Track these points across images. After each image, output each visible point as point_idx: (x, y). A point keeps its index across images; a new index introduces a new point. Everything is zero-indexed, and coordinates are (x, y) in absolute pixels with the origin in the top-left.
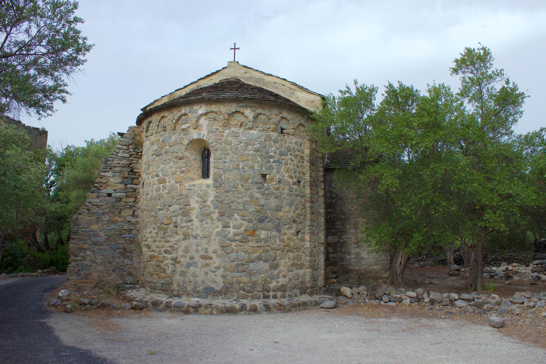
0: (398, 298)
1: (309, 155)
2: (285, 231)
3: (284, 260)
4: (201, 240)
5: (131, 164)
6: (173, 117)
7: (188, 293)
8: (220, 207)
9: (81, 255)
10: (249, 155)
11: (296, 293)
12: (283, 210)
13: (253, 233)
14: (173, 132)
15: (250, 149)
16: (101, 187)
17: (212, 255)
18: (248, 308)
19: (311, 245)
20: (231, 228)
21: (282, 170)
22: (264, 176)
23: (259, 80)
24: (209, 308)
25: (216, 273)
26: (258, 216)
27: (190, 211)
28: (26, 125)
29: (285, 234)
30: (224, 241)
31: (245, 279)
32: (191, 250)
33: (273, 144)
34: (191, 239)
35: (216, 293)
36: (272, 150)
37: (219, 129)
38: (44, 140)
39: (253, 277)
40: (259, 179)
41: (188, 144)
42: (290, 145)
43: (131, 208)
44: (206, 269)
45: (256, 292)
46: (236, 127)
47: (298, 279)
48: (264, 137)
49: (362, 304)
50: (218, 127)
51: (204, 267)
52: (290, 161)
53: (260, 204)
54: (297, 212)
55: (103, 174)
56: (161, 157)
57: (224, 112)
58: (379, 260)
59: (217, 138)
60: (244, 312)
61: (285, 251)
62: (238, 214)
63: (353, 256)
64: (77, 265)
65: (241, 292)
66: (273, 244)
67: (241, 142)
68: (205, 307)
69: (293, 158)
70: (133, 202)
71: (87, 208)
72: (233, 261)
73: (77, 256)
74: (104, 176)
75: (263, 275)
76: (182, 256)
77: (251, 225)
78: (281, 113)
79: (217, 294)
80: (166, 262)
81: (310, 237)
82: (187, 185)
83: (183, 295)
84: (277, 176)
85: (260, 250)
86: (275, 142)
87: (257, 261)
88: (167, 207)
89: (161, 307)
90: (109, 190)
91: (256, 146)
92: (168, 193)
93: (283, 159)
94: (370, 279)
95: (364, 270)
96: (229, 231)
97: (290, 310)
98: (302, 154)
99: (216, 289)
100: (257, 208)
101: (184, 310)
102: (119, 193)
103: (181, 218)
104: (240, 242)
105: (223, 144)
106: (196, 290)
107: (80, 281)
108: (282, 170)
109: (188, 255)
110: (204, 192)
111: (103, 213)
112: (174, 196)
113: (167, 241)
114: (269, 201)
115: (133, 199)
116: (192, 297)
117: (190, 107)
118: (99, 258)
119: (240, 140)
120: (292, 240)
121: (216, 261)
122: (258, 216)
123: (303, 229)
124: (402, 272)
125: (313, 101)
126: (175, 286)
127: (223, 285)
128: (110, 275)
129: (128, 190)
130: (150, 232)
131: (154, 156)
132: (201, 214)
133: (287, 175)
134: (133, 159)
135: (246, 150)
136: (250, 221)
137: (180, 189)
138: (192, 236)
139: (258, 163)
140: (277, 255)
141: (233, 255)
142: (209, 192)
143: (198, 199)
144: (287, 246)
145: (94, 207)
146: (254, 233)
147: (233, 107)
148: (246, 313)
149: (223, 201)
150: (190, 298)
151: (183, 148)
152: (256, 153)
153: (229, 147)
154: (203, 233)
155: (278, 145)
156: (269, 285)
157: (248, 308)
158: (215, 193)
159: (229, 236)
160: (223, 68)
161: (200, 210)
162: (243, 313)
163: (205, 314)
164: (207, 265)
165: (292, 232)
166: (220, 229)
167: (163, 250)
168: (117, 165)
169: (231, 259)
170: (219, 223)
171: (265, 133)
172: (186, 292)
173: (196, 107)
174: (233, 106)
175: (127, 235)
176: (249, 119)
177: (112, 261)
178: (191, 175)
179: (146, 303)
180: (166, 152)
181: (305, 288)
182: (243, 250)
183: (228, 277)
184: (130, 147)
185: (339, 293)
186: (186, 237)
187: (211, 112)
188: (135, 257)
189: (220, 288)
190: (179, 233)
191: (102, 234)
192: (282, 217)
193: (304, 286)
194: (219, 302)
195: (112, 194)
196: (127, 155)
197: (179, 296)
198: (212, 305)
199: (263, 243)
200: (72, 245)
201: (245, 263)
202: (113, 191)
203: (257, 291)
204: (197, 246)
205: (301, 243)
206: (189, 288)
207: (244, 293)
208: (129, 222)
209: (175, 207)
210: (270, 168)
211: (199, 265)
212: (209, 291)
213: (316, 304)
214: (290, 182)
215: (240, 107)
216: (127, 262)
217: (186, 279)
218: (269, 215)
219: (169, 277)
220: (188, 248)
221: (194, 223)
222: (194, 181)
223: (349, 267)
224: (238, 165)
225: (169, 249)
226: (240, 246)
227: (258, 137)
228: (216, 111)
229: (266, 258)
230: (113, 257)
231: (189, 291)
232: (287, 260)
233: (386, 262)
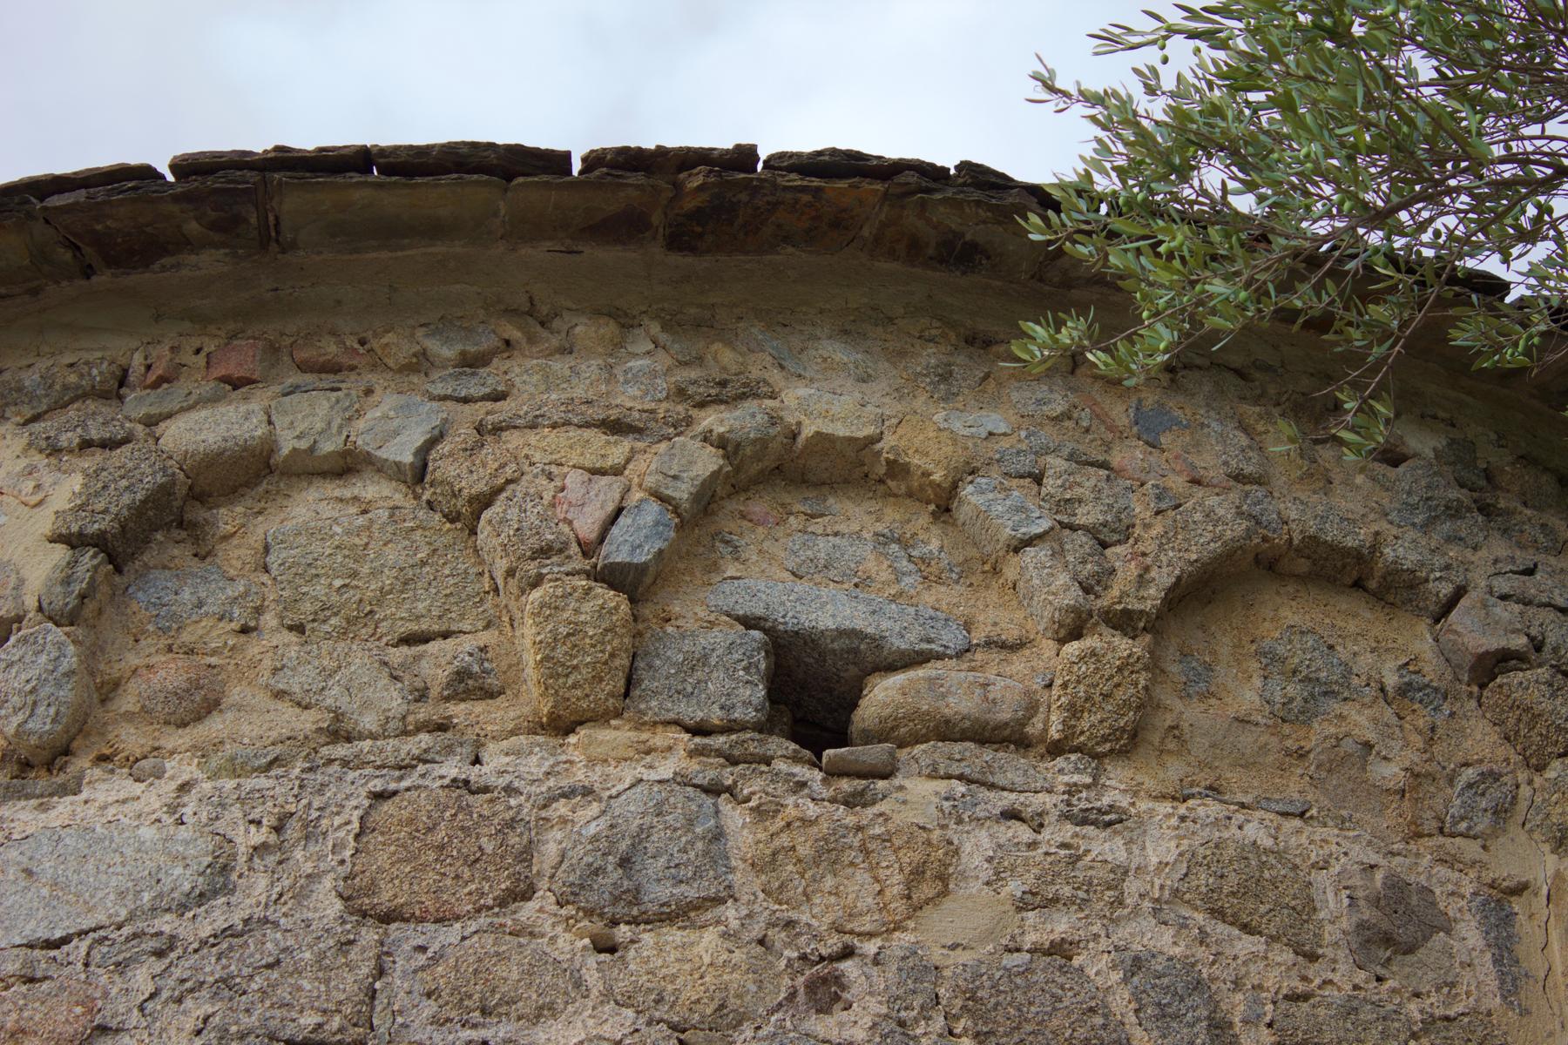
33: (569, 944)
42: (1061, 925)
227: (183, 879)
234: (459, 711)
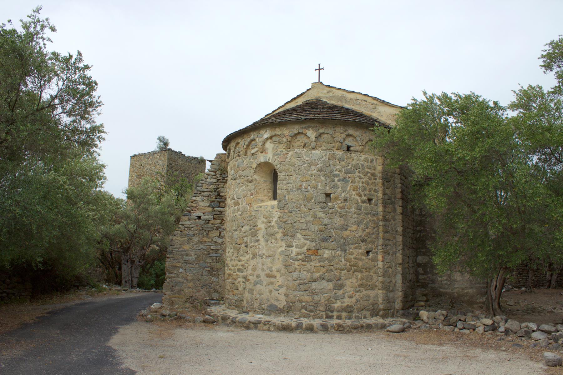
0: (472, 325)
1: (381, 171)
2: (351, 250)
3: (350, 280)
4: (266, 259)
5: (217, 188)
6: (244, 142)
7: (255, 310)
8: (283, 227)
9: (175, 272)
10: (312, 175)
11: (365, 315)
12: (349, 229)
13: (316, 253)
14: (245, 157)
15: (313, 169)
16: (192, 210)
17: (276, 273)
18: (304, 326)
19: (384, 265)
20: (294, 247)
21: (349, 188)
22: (328, 195)
23: (342, 98)
24: (267, 325)
25: (280, 292)
26: (321, 235)
27: (258, 231)
28: (186, 155)
29: (351, 254)
30: (287, 260)
31: (307, 298)
32: (257, 269)
33: (338, 162)
34: (258, 258)
35: (279, 311)
37: (283, 152)
38: (203, 168)
39: (316, 296)
40: (322, 198)
41: (256, 168)
42: (358, 162)
43: (218, 229)
44: (270, 287)
45: (318, 312)
46: (299, 149)
47: (369, 300)
48: (327, 156)
49: (435, 330)
50: (282, 149)
51: (269, 285)
52: (358, 178)
53: (323, 224)
54: (367, 231)
55: (194, 198)
57: (287, 134)
58: (474, 283)
59: (281, 160)
60: (300, 330)
61: (352, 271)
62: (301, 234)
63: (445, 278)
64: (171, 281)
65: (304, 311)
66: (337, 264)
67: (304, 162)
68: (263, 324)
69: (361, 175)
70: (219, 224)
71: (180, 230)
72: (296, 280)
74: (195, 200)
75: (326, 295)
77: (314, 244)
78: (346, 131)
79: (280, 311)
80: (239, 279)
81: (382, 257)
82: (255, 206)
83: (250, 311)
84: (343, 195)
85: (323, 270)
86: (340, 160)
88: (240, 227)
89: (229, 321)
90: (199, 213)
91: (319, 166)
92: (240, 215)
93: (349, 177)
94: (463, 304)
95: (457, 293)
96: (292, 250)
97: (350, 332)
98: (373, 171)
99: (279, 307)
100: (320, 227)
101: (246, 325)
103: (250, 238)
104: (303, 261)
105: (287, 165)
106: (261, 307)
107: (174, 296)
108: (349, 188)
109: (256, 274)
110: (269, 213)
112: (246, 218)
113: (240, 260)
114: (333, 220)
115: (219, 221)
116: (258, 314)
117: (257, 132)
118: (190, 275)
119: (303, 160)
120: (360, 260)
121: (280, 280)
122: (321, 235)
123: (375, 249)
124: (497, 297)
126: (245, 303)
127: (285, 303)
128: (199, 291)
129: (215, 213)
132: (267, 234)
133: (354, 193)
134: (220, 184)
136: (312, 241)
137: (250, 211)
138: (259, 256)
139: (322, 182)
140: (342, 275)
141: (296, 275)
142: (273, 212)
143: (264, 220)
144: (354, 266)
145: (186, 229)
146: (317, 253)
147: (296, 129)
148: (301, 332)
149: (286, 221)
150: (255, 315)
151: (253, 171)
152: (319, 172)
153: (292, 168)
154: (268, 252)
155: (343, 163)
156: (333, 305)
157: (304, 326)
158: (279, 214)
160: (308, 90)
161: (265, 231)
162: (298, 331)
163: (264, 330)
164: (271, 283)
165: (360, 251)
166: (283, 249)
167: (236, 268)
168: (206, 190)
169: (294, 279)
170: (283, 243)
171: (329, 152)
172: (253, 308)
173: (262, 132)
174: (295, 128)
175: (214, 255)
176: (311, 140)
177: (200, 278)
178: (260, 197)
179: (217, 318)
181: (377, 310)
182: (305, 269)
183: (291, 296)
184: (217, 172)
185: (417, 317)
186: (254, 256)
187: (275, 135)
188: (220, 275)
189: (282, 306)
190: (249, 252)
191: (192, 253)
192: (348, 236)
193: (376, 308)
194: (278, 320)
195: (201, 217)
196: (215, 181)
197: (247, 312)
198: (270, 322)
199: (326, 262)
200: (168, 263)
201: (307, 282)
202: (202, 214)
203: (319, 310)
204: (263, 265)
205: (373, 263)
206: (256, 305)
207: (306, 312)
208: (216, 242)
209: (246, 228)
210: (335, 187)
212: (273, 310)
213: (383, 327)
214: (357, 200)
215: (302, 128)
216: (213, 280)
217: (253, 296)
218: (334, 234)
219: (241, 294)
220: (255, 267)
221: (260, 243)
222: (264, 202)
223: (441, 290)
224: (301, 186)
225: (241, 267)
226: (302, 265)
227: (321, 157)
228: (279, 134)
229: (329, 278)
230: (202, 275)
231: (256, 308)
232: (354, 280)
233: (481, 285)
234: (333, 148)
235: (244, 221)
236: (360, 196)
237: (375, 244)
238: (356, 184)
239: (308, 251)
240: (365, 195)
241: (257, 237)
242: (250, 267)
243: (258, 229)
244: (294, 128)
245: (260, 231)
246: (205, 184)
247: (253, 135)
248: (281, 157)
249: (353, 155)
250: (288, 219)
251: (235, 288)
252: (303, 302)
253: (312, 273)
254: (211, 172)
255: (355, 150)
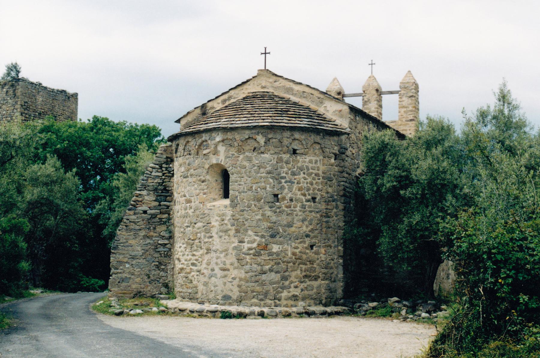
4: (219, 254)
5: (163, 182)
6: (195, 142)
8: (236, 225)
9: (121, 268)
12: (295, 225)
13: (265, 247)
14: (196, 156)
16: (137, 204)
22: (276, 196)
25: (233, 283)
27: (211, 229)
34: (212, 253)
36: (284, 171)
40: (271, 199)
41: (209, 168)
42: (303, 164)
44: (224, 280)
46: (250, 152)
48: (275, 160)
50: (234, 153)
52: (303, 179)
56: (187, 179)
57: (238, 139)
59: (233, 162)
61: (297, 264)
62: (252, 230)
66: (284, 257)
67: (254, 165)
73: (117, 269)
74: (140, 195)
75: (275, 285)
76: (205, 268)
77: (264, 240)
80: (193, 273)
85: (272, 263)
87: (269, 272)
88: (193, 224)
90: (145, 208)
93: (295, 179)
102: (153, 211)
109: (210, 267)
111: (139, 229)
119: (254, 163)
123: (318, 243)
125: (341, 111)
130: (180, 247)
131: (182, 177)
133: (299, 193)
135: (258, 173)
136: (263, 236)
141: (248, 267)
145: (132, 224)
146: (266, 247)
151: (205, 171)
153: (243, 170)
157: (256, 313)
158: (232, 212)
159: (244, 250)
160: (253, 77)
164: (225, 276)
165: (305, 246)
167: (190, 262)
169: (246, 271)
172: (208, 299)
173: (214, 134)
180: (191, 175)
182: (256, 262)
186: (208, 251)
187: (227, 139)
188: (169, 270)
190: (203, 247)
195: (148, 212)
196: (160, 174)
199: (275, 256)
205: (316, 256)
208: (163, 236)
209: (199, 225)
210: (282, 188)
211: (219, 276)
214: (302, 200)
215: (252, 133)
216: (162, 275)
219: (195, 287)
224: (252, 187)
225: (195, 262)
229: (277, 270)
235: (197, 218)
236: (304, 195)
237: (319, 239)
238: (301, 185)
239: (258, 246)
240: (309, 195)
241: (211, 233)
242: (205, 261)
243: (211, 226)
244: (245, 133)
245: (214, 228)
246: (150, 178)
247: (205, 137)
248: (232, 160)
249: (298, 157)
250: (239, 217)
251: (189, 281)
252: (254, 292)
253: (261, 266)
254: (156, 164)
255: (301, 153)
